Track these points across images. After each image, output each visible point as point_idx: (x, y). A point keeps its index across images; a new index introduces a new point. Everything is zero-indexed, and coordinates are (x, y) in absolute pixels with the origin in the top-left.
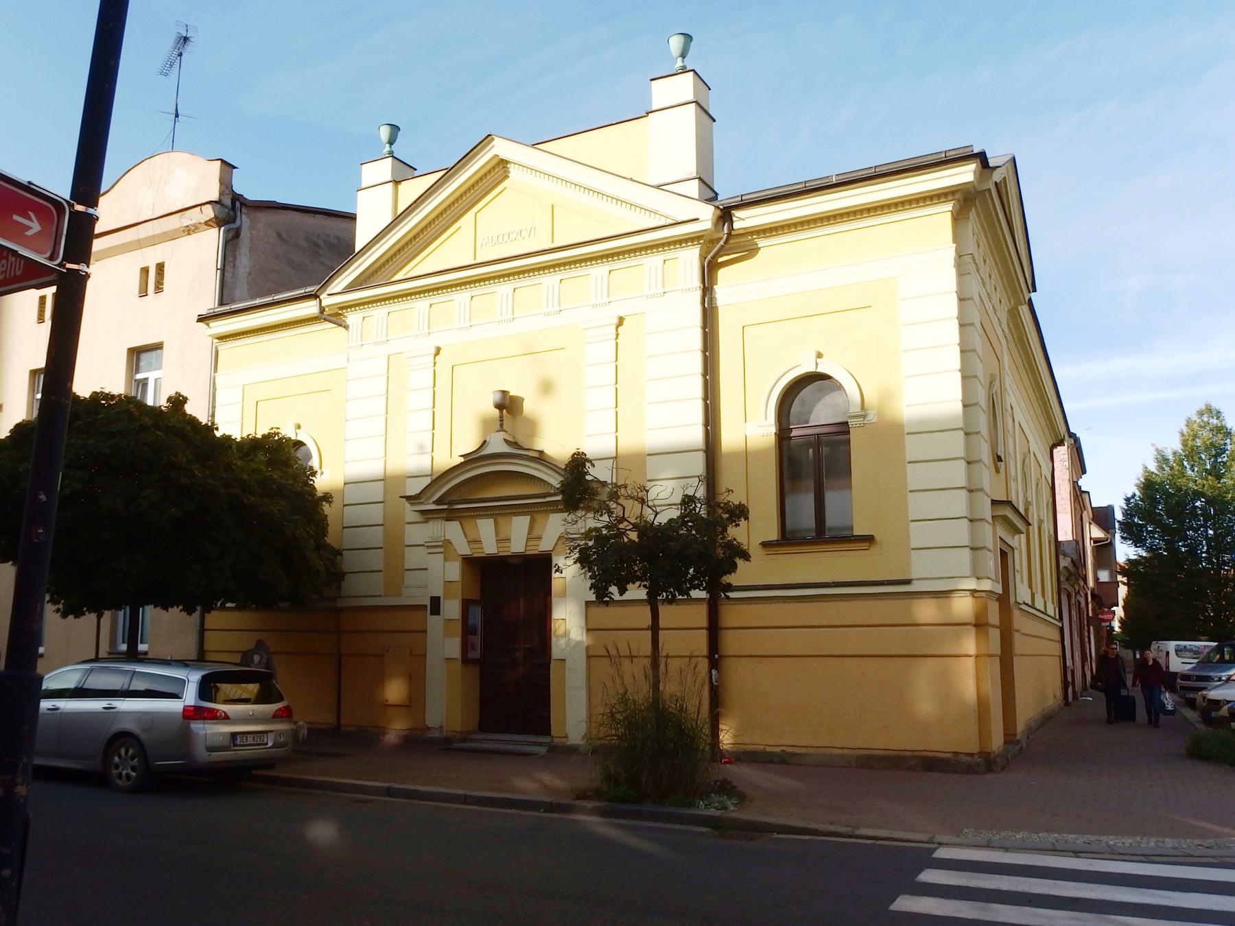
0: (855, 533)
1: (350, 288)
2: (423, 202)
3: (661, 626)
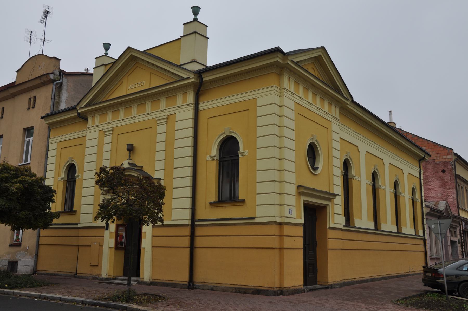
0: (239, 199)
1: (87, 106)
2: (241, 63)
3: (302, 250)
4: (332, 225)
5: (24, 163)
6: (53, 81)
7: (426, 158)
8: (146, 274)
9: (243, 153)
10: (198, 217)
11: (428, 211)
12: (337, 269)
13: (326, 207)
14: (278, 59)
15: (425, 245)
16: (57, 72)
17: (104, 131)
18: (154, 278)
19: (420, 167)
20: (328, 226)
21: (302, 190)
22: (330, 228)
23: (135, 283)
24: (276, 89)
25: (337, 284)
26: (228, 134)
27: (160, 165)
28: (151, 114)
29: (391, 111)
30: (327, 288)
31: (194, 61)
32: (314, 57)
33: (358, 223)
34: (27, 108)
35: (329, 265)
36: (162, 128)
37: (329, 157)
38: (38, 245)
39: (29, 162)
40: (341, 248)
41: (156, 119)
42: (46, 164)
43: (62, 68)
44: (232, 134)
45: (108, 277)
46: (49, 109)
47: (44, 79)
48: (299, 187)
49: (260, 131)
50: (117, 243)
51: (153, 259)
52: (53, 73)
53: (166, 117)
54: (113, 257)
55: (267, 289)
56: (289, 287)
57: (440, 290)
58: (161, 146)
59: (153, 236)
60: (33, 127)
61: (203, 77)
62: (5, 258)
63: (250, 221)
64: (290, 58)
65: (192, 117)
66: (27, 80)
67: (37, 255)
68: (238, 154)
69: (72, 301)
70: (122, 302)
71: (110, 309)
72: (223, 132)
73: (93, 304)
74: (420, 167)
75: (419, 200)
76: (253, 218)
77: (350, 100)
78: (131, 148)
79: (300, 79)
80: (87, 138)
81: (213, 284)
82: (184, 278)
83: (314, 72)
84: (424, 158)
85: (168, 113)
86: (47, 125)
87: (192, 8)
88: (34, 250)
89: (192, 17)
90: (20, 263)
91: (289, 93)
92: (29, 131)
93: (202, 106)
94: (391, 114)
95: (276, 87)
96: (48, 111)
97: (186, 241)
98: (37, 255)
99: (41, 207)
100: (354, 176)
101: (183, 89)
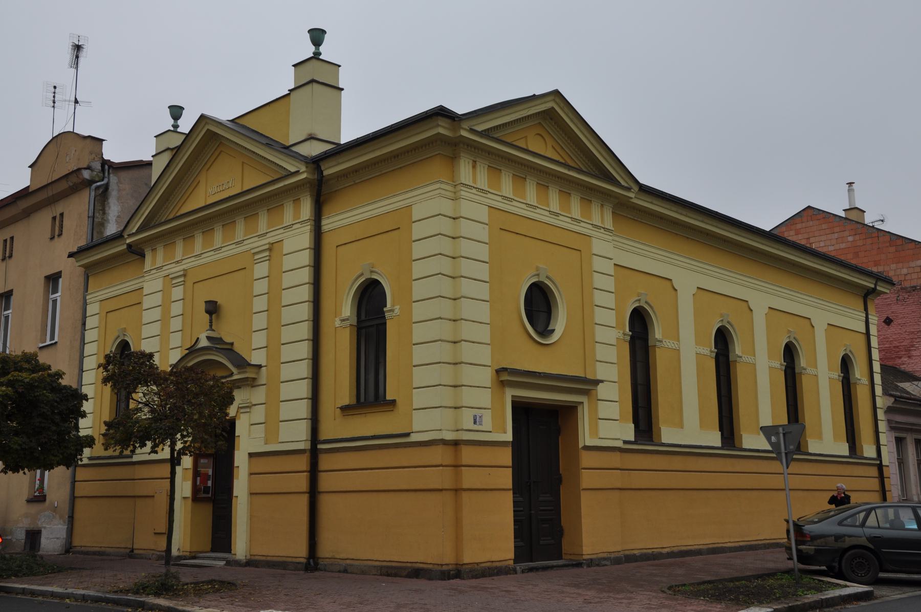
0: (388, 398)
1: (139, 231)
4: (589, 442)
5: (48, 342)
6: (89, 183)
7: (878, 288)
8: (241, 547)
9: (392, 311)
10: (323, 436)
11: (890, 404)
12: (599, 525)
13: (576, 407)
14: (441, 131)
15: (881, 477)
16: (97, 166)
17: (171, 276)
18: (254, 552)
19: (866, 309)
20: (581, 445)
21: (505, 376)
22: (586, 448)
23: (223, 563)
24: (443, 186)
25: (605, 559)
26: (367, 275)
27: (259, 340)
28: (245, 242)
29: (850, 184)
30: (579, 565)
31: (311, 138)
32: (539, 113)
33: (668, 435)
34: (49, 236)
35: (583, 521)
36: (261, 269)
37: (585, 307)
38: (73, 498)
39: (56, 339)
40: (619, 486)
41: (253, 251)
42: (83, 343)
43: (106, 157)
44: (375, 277)
45: (181, 554)
46: (84, 237)
47: (74, 180)
48: (499, 372)
49: (418, 269)
50: (195, 490)
51: (252, 517)
52: (89, 168)
53: (267, 247)
54: (190, 515)
55: (430, 566)
56: (477, 564)
57: (824, 568)
58: (260, 304)
59: (251, 474)
60: (61, 272)
61: (323, 168)
62: (21, 525)
63: (400, 441)
64: (465, 125)
65: (308, 246)
66: (45, 183)
67: (71, 518)
68: (383, 313)
69: (69, 596)
70: (148, 594)
71: (119, 608)
72: (359, 273)
73: (97, 600)
74: (866, 309)
75: (865, 381)
76: (407, 435)
77: (636, 188)
78: (213, 309)
79: (498, 162)
80: (145, 292)
81: (348, 562)
82: (300, 551)
83: (546, 143)
84: (874, 290)
85: (272, 240)
86: (83, 269)
87: (309, 31)
88: (66, 507)
89: (309, 50)
90: (44, 534)
91: (474, 191)
92: (53, 280)
93: (328, 224)
94: (853, 190)
95: (442, 182)
96: (83, 243)
97: (302, 482)
98: (71, 518)
99: (54, 428)
100: (661, 341)
101: (292, 192)
